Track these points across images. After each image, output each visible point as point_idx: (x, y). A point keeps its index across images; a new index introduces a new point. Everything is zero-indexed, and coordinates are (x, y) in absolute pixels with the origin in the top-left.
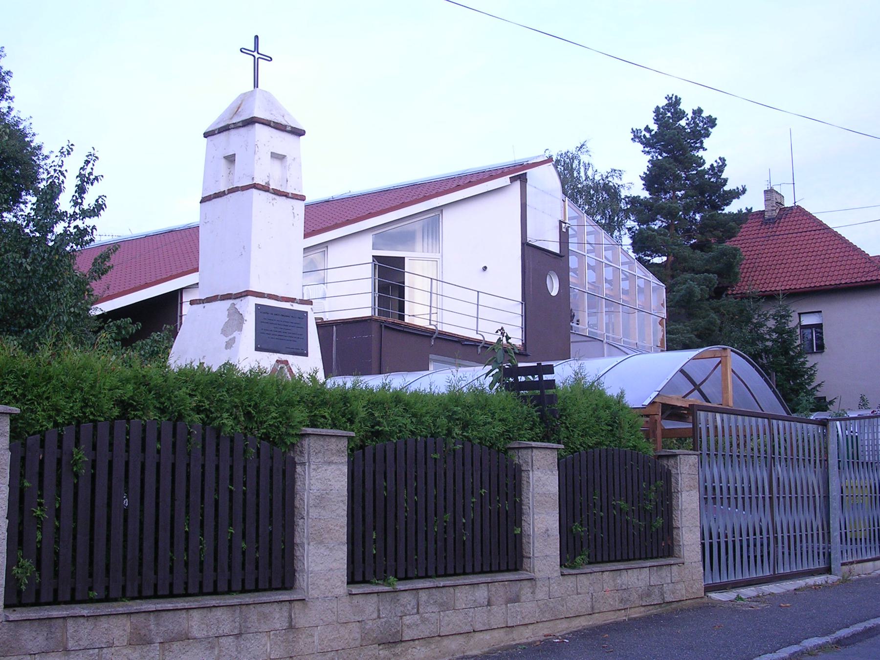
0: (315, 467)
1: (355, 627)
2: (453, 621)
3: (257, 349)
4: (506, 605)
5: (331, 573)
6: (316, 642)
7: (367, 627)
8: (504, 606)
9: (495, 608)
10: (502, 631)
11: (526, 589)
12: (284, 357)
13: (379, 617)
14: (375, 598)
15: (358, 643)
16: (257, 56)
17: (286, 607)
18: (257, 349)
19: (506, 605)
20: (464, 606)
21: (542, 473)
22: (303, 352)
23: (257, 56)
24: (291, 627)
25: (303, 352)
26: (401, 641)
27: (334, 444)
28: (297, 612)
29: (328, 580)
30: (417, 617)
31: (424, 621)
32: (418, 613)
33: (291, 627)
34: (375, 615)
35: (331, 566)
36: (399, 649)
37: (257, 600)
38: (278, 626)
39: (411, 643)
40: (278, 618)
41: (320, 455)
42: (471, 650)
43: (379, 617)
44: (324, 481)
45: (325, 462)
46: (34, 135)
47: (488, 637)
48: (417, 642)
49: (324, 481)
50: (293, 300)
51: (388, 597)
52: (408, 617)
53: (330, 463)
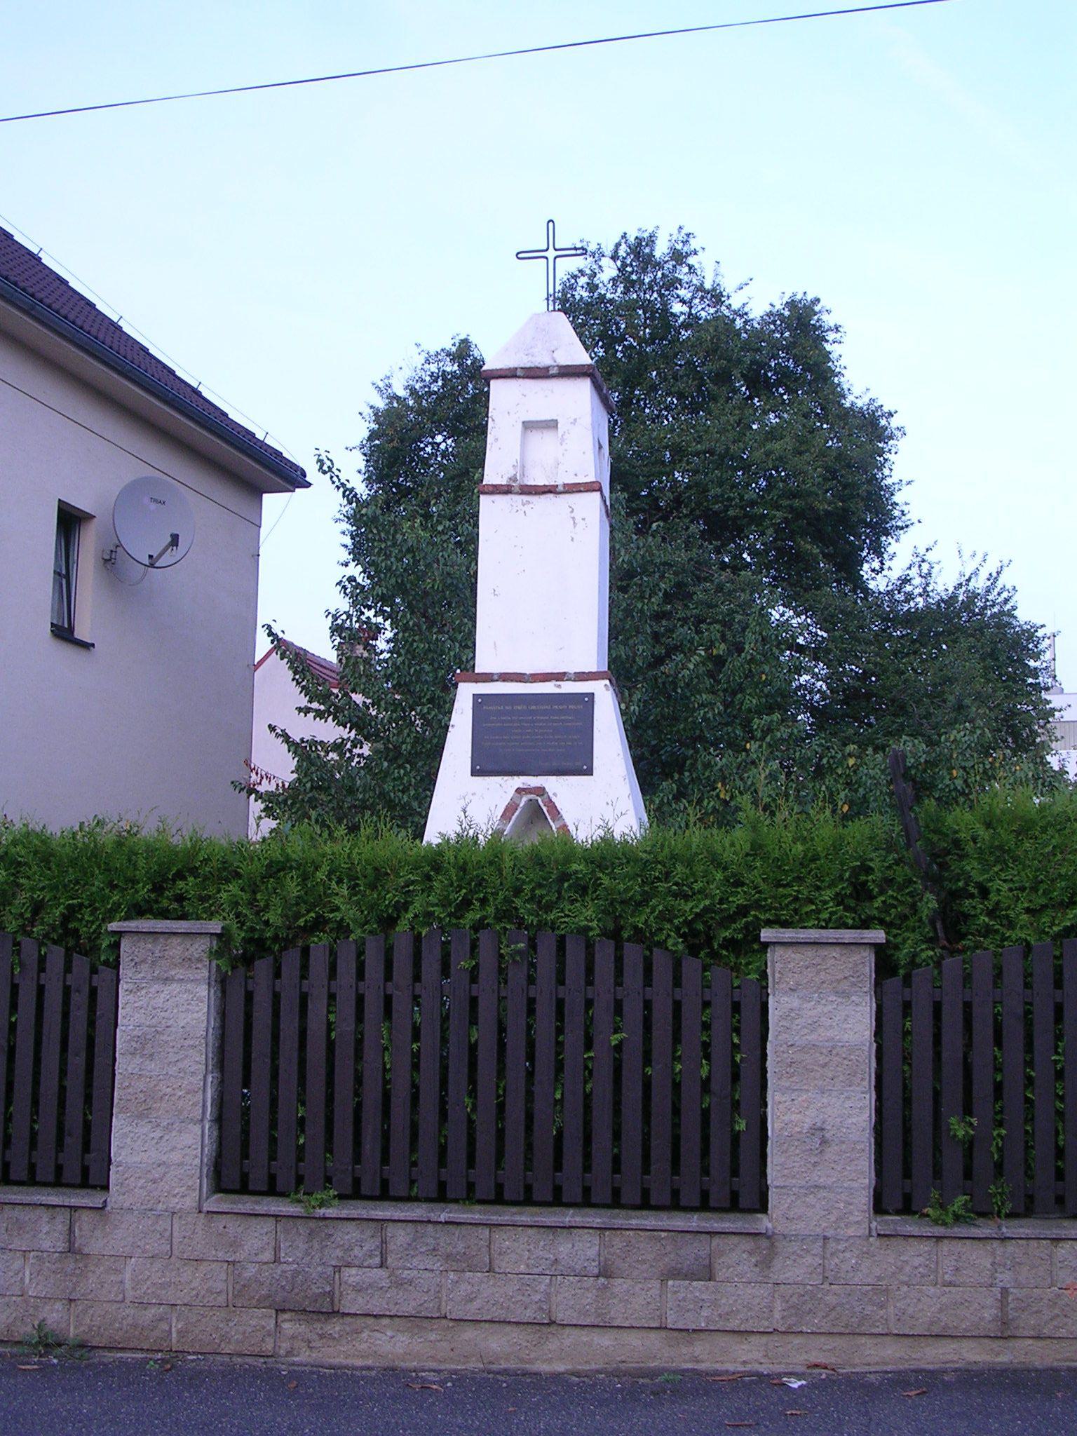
0: (131, 986)
1: (221, 1272)
2: (487, 1293)
3: (475, 773)
4: (663, 1281)
5: (162, 1170)
6: (128, 1285)
7: (247, 1275)
8: (657, 1284)
9: (619, 1285)
10: (653, 1335)
11: (736, 1259)
12: (533, 781)
13: (277, 1260)
14: (269, 1224)
15: (221, 1299)
16: (551, 254)
17: (62, 1218)
18: (475, 773)
19: (663, 1281)
20: (522, 1268)
21: (804, 999)
22: (580, 764)
23: (551, 254)
24: (71, 1249)
25: (580, 764)
26: (552, 1323)
27: (176, 948)
28: (86, 1227)
29: (154, 1181)
30: (382, 1273)
31: (400, 1284)
32: (382, 1265)
33: (71, 1249)
34: (268, 1256)
35: (164, 1158)
36: (335, 1327)
37: (27, 1199)
38: (46, 1245)
39: (370, 1321)
40: (49, 1233)
41: (144, 967)
42: (550, 1361)
43: (277, 1260)
44: (166, 1011)
45: (156, 979)
46: (891, 415)
47: (636, 1342)
48: (385, 1321)
49: (166, 1011)
50: (560, 677)
51: (303, 1228)
52: (354, 1271)
53: (166, 980)
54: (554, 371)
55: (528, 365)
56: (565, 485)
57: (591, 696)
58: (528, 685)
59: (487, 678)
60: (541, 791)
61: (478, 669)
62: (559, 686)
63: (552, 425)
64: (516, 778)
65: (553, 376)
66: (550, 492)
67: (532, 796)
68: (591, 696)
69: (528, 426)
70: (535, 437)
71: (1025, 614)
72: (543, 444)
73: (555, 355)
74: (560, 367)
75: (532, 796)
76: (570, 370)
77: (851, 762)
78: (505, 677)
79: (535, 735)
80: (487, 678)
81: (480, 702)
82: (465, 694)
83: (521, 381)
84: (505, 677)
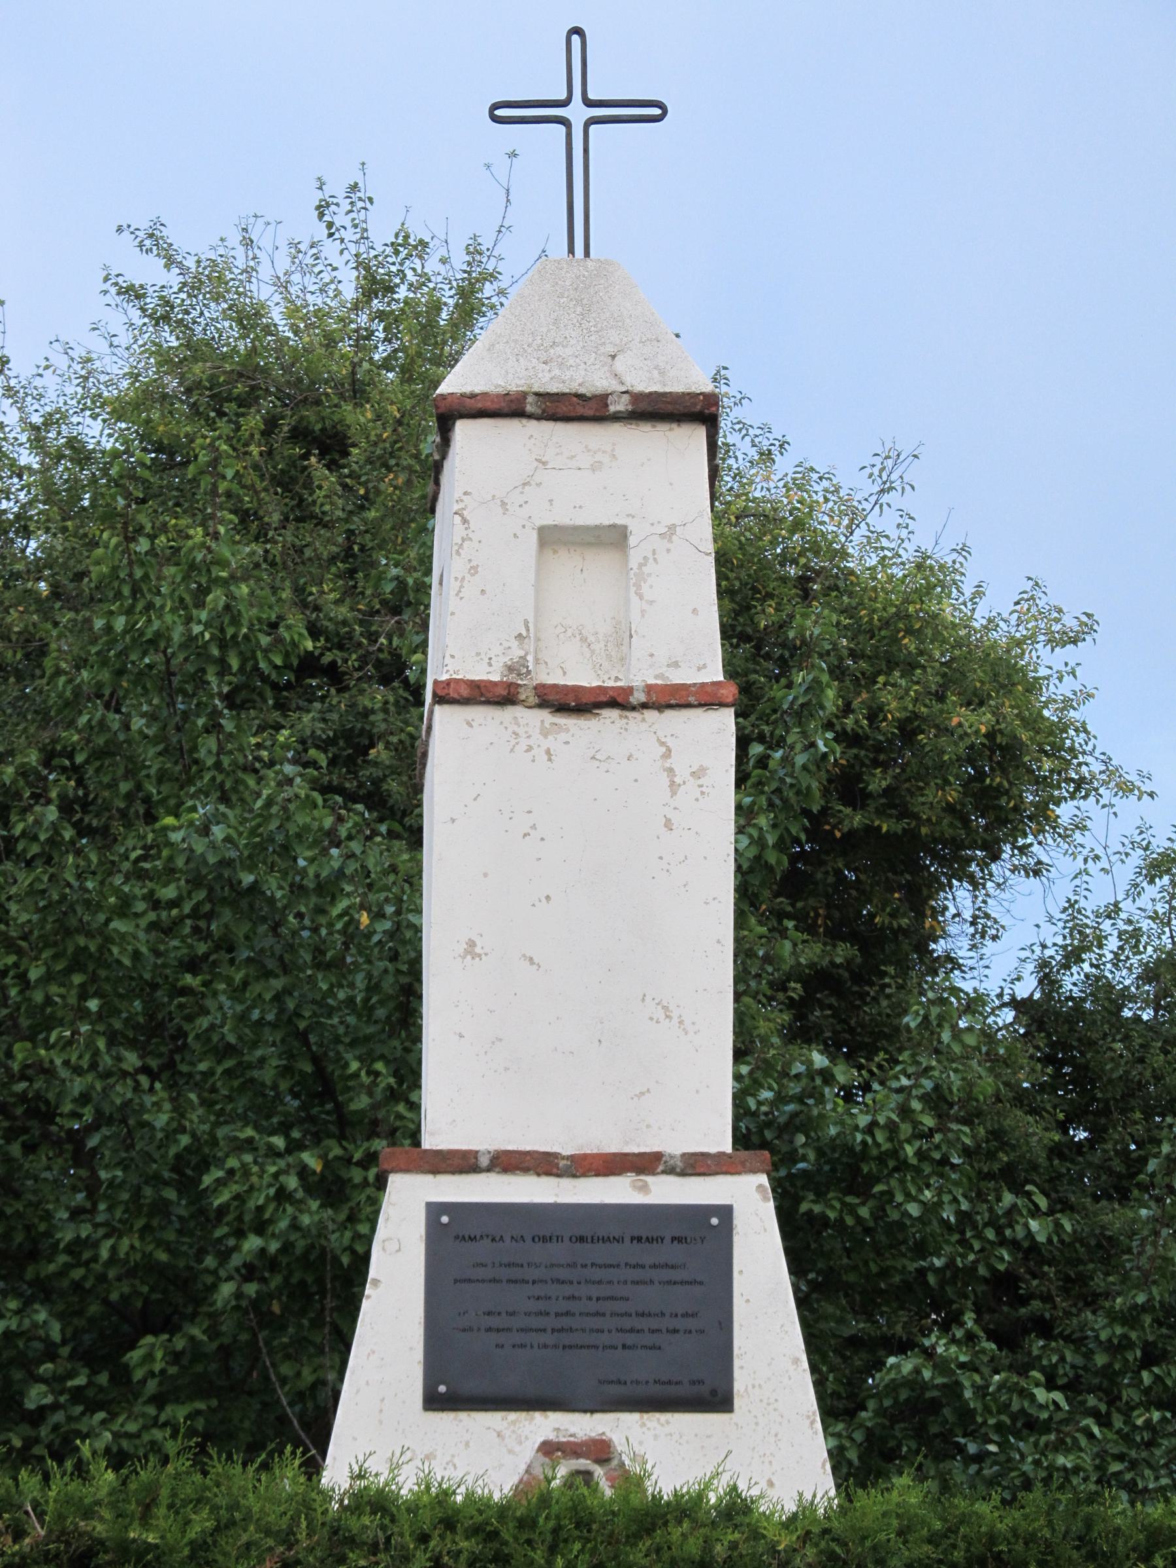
3: (434, 1402)
18: (434, 1402)
50: (645, 1164)
54: (619, 405)
55: (554, 388)
56: (649, 688)
57: (726, 1213)
58: (566, 1182)
59: (461, 1163)
60: (601, 1451)
61: (429, 1142)
62: (644, 1188)
63: (614, 538)
64: (538, 1416)
65: (616, 418)
66: (613, 704)
67: (584, 1463)
68: (726, 1213)
69: (551, 538)
70: (566, 564)
71: (987, 600)
72: (584, 585)
73: (620, 365)
74: (637, 397)
75: (584, 1463)
76: (662, 407)
77: (93, 1005)
78: (508, 1163)
79: (579, 1301)
80: (461, 1163)
81: (449, 1229)
82: (406, 1207)
83: (532, 426)
84: (508, 1163)
